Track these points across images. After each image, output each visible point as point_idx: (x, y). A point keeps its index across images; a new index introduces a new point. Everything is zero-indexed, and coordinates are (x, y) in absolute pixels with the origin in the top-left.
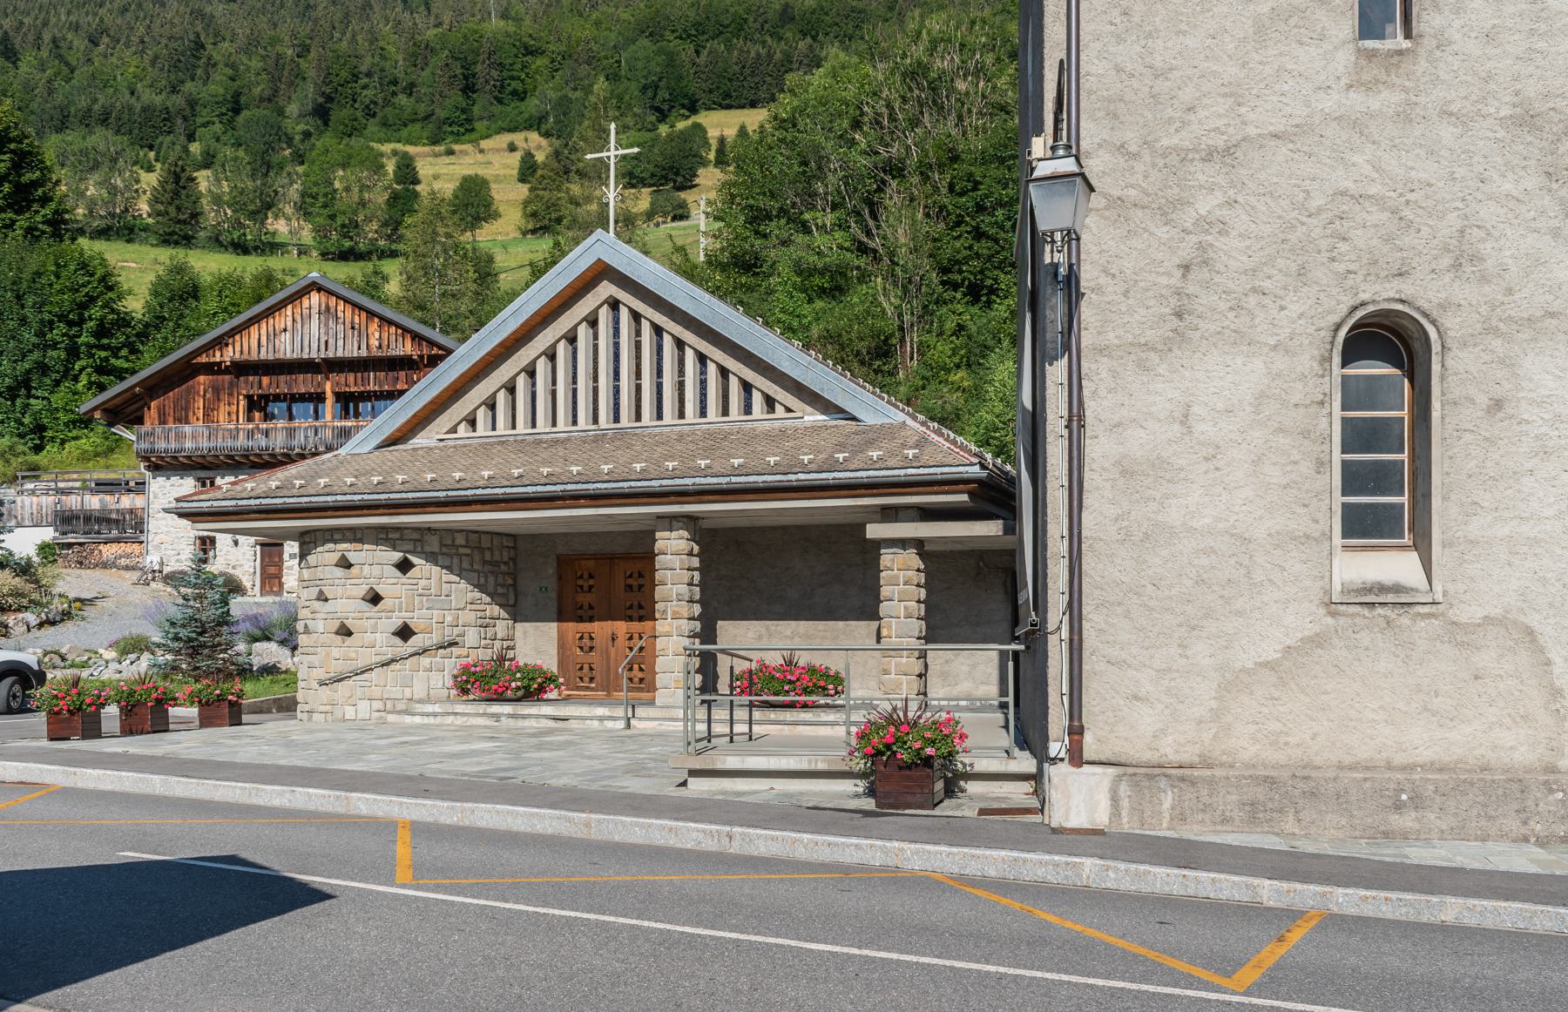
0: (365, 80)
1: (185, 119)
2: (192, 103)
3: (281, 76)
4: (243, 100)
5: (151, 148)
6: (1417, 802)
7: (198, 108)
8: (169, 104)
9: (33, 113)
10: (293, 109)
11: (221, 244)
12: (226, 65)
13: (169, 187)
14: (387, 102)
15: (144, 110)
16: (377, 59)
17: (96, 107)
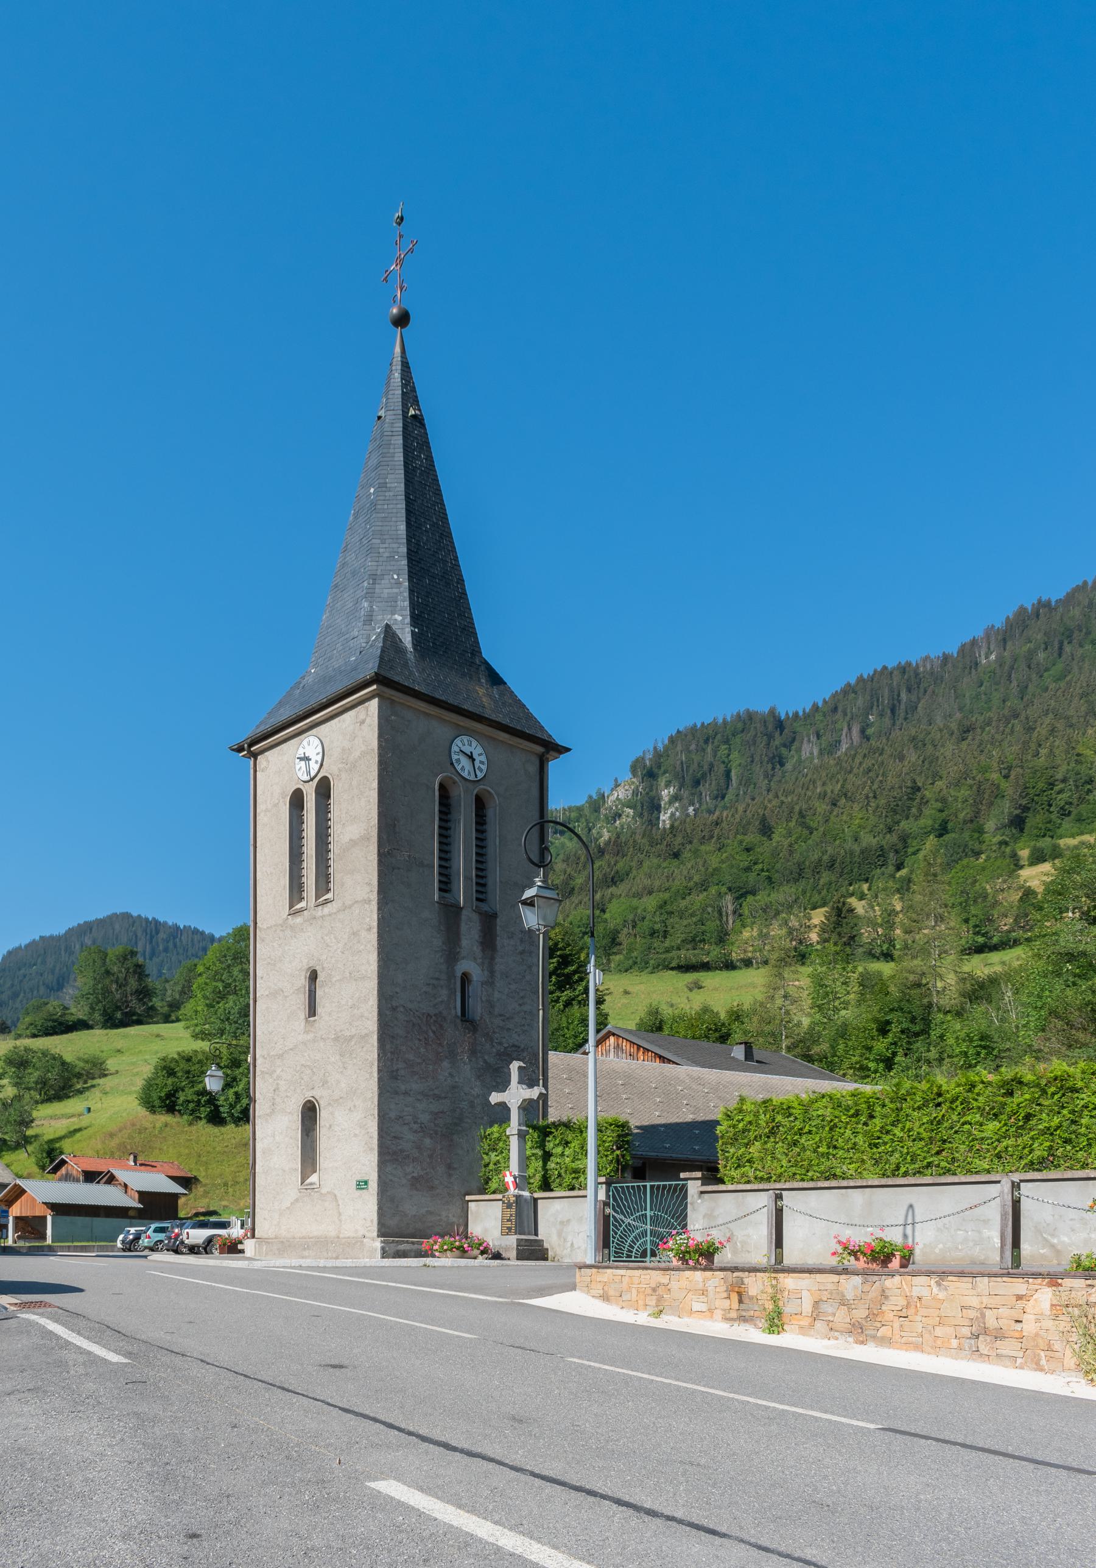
0: (1062, 786)
1: (897, 852)
2: (904, 839)
3: (985, 796)
4: (950, 826)
5: (867, 880)
6: (308, 1248)
7: (909, 841)
8: (884, 843)
9: (777, 871)
10: (990, 825)
11: (874, 956)
12: (937, 800)
13: (834, 919)
14: (1081, 800)
15: (862, 852)
16: (1073, 765)
17: (825, 857)
